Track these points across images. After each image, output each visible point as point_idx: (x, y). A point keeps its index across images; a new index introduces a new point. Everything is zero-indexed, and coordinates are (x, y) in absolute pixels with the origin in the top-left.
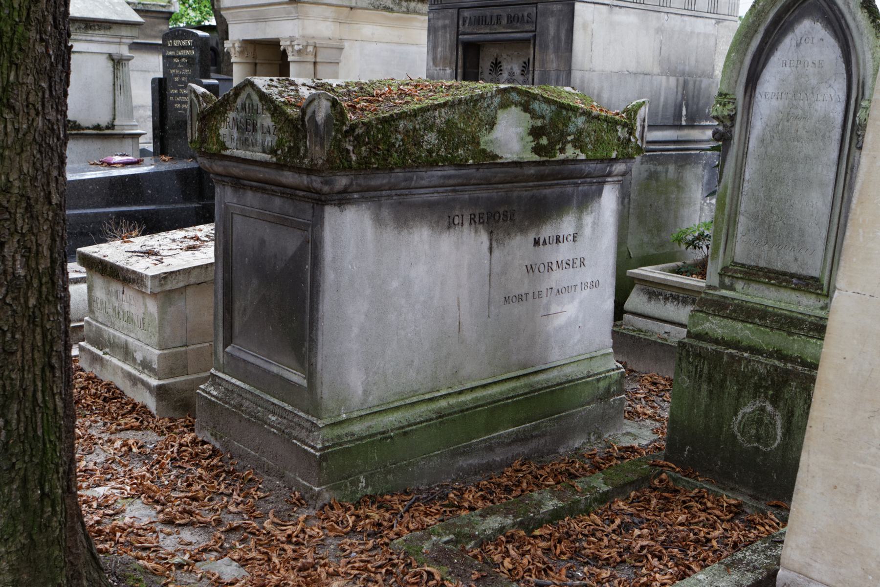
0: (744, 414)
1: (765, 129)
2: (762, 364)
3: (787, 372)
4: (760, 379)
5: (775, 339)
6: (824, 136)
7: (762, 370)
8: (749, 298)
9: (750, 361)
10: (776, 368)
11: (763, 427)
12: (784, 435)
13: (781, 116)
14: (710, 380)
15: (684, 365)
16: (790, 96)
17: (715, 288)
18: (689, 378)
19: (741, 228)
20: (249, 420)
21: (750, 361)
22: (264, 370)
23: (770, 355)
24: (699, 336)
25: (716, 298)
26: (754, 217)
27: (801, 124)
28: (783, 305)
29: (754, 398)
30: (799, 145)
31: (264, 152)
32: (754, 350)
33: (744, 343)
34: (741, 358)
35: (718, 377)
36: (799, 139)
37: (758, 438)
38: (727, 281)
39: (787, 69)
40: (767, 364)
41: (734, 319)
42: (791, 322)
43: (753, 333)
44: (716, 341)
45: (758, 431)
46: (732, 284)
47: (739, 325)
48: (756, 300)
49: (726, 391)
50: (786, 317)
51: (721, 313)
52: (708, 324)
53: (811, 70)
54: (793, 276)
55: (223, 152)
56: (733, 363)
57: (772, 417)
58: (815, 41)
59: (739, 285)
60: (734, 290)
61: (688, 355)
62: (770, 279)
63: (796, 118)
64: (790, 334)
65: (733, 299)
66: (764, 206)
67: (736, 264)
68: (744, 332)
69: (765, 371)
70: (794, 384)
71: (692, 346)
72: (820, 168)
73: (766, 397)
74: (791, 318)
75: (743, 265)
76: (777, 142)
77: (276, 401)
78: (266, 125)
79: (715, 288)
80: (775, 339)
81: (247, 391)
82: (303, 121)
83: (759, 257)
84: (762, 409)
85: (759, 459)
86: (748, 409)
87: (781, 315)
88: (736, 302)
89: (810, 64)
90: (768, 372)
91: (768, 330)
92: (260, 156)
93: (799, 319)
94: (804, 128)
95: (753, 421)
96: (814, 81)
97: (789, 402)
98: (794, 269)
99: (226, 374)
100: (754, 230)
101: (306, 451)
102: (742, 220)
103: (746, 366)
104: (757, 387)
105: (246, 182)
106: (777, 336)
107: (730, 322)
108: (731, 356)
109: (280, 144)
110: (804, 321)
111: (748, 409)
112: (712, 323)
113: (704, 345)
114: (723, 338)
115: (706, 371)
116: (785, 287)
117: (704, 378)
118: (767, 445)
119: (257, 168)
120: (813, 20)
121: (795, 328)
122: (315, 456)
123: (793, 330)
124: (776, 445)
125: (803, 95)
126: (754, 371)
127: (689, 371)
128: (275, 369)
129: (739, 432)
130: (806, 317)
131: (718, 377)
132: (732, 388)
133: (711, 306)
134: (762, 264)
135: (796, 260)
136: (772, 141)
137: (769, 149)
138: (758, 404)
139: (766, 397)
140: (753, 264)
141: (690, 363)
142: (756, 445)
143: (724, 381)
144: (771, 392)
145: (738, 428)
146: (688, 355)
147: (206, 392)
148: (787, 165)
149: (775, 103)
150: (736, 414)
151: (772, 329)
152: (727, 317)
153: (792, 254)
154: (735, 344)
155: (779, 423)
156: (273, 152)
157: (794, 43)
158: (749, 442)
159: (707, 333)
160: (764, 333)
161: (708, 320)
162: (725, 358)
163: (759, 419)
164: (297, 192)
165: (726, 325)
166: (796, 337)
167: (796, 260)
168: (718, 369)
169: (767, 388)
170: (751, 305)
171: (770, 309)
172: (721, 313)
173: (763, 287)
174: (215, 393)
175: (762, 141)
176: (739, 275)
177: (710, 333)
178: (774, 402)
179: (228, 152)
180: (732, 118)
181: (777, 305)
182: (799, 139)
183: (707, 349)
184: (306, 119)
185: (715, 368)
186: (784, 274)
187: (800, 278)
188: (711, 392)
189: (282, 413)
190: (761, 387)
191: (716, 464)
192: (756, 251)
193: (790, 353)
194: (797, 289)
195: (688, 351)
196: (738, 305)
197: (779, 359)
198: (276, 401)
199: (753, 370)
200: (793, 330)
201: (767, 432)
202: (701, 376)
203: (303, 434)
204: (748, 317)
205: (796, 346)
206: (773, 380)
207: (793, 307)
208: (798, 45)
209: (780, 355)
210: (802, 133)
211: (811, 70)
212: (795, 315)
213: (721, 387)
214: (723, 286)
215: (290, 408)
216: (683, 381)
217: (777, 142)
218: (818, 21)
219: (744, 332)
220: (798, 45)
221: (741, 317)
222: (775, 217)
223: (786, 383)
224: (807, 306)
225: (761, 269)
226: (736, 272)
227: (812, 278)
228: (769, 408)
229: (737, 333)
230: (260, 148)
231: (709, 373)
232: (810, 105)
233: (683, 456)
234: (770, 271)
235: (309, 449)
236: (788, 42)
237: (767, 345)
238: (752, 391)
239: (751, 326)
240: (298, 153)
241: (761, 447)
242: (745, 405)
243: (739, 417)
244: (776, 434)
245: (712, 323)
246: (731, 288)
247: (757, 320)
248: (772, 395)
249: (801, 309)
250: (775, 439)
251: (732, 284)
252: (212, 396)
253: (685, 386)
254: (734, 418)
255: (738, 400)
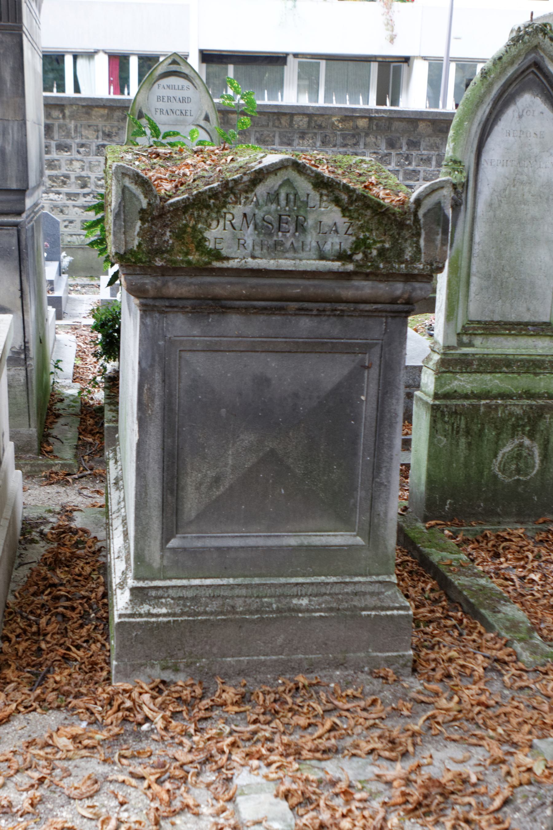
0: (504, 454)
1: (492, 194)
2: (517, 407)
3: (542, 407)
4: (518, 419)
5: (524, 382)
6: (548, 199)
7: (519, 411)
8: (491, 351)
9: (506, 406)
10: (531, 406)
11: (522, 461)
12: (542, 461)
13: (507, 181)
14: (468, 432)
15: (439, 426)
16: (515, 163)
17: (453, 348)
18: (445, 436)
19: (473, 288)
20: (261, 619)
21: (506, 406)
22: (269, 549)
23: (520, 397)
24: (447, 396)
25: (457, 357)
26: (487, 276)
27: (527, 189)
28: (524, 351)
29: (513, 437)
30: (526, 207)
31: (322, 257)
32: (503, 396)
33: (494, 392)
34: (497, 406)
35: (476, 428)
36: (525, 202)
37: (518, 471)
38: (465, 339)
39: (511, 138)
40: (522, 405)
41: (481, 373)
42: (534, 364)
43: (501, 380)
44: (466, 397)
45: (517, 465)
46: (470, 341)
47: (488, 377)
48: (499, 351)
49: (485, 438)
50: (528, 361)
51: (468, 370)
52: (456, 383)
53: (533, 140)
54: (527, 324)
55: (217, 264)
56: (490, 412)
57: (529, 449)
58: (536, 113)
59: (478, 341)
60: (473, 346)
61: (443, 415)
62: (509, 330)
63: (522, 183)
64: (536, 374)
65: (473, 355)
66: (496, 265)
67: (472, 322)
68: (494, 382)
69: (522, 411)
70: (548, 416)
71: (447, 406)
72: (546, 227)
73: (524, 434)
74: (532, 361)
75: (479, 322)
76: (505, 206)
77: (301, 580)
78: (327, 220)
79: (453, 348)
80: (524, 382)
81: (231, 587)
82: (416, 214)
83: (493, 312)
84: (521, 445)
85: (520, 490)
86: (507, 449)
87: (521, 361)
88: (477, 356)
89: (533, 135)
90: (524, 411)
91: (516, 375)
92: (312, 264)
93: (539, 361)
94: (530, 192)
95: (512, 457)
96: (536, 150)
97: (545, 432)
98: (527, 318)
99: (170, 579)
100: (487, 288)
101: (392, 616)
102: (474, 279)
103: (503, 411)
104: (514, 427)
105: (229, 303)
106: (524, 379)
107: (478, 376)
108: (488, 406)
109: (359, 245)
110: (543, 361)
111: (507, 449)
112: (461, 381)
113: (454, 402)
114: (472, 392)
115: (463, 426)
116: (525, 335)
117: (461, 432)
118: (527, 475)
119: (291, 282)
120: (533, 94)
121: (540, 368)
122: (407, 616)
123: (538, 371)
124: (535, 472)
125: (527, 163)
126: (511, 414)
127: (445, 430)
128: (293, 541)
129: (500, 471)
130: (543, 358)
131: (476, 428)
132: (490, 433)
133: (456, 365)
134: (497, 318)
135: (528, 310)
136: (500, 206)
137: (498, 212)
138: (517, 442)
139: (524, 434)
140: (488, 319)
141: (445, 422)
142: (516, 477)
143: (481, 430)
144: (528, 428)
145: (499, 468)
146: (443, 415)
147: (140, 615)
148: (515, 227)
149: (501, 170)
150: (495, 456)
151: (519, 373)
152: (475, 372)
153: (525, 305)
154: (486, 395)
155: (537, 452)
156: (342, 257)
157: (516, 114)
158: (510, 477)
159: (456, 391)
160: (512, 378)
161: (456, 379)
162: (482, 409)
163: (518, 455)
164: (362, 306)
165: (475, 380)
166: (542, 376)
167: (528, 310)
168: (475, 420)
169: (524, 426)
170: (491, 356)
171: (511, 357)
172: (468, 370)
173: (501, 339)
174: (164, 610)
175: (491, 205)
176: (480, 332)
177: (459, 391)
178: (531, 436)
179: (233, 264)
180: (465, 186)
181: (518, 352)
182: (525, 202)
183: (463, 405)
184: (421, 213)
185: (472, 420)
186: (519, 324)
187: (534, 324)
188: (469, 444)
189: (317, 591)
190: (518, 426)
191: (479, 506)
192: (490, 307)
193: (537, 391)
194: (536, 335)
195: (442, 412)
196: (480, 359)
197: (528, 398)
198: (301, 580)
199: (510, 414)
200: (538, 371)
201: (526, 463)
202: (458, 432)
203: (372, 601)
204: (495, 368)
205: (542, 384)
206: (529, 418)
207: (533, 352)
208: (520, 117)
209: (529, 395)
210: (528, 196)
211: (533, 140)
212: (533, 357)
213: (480, 436)
214: (461, 344)
215: (333, 579)
216: (440, 441)
217: (505, 206)
218: (537, 95)
219: (494, 382)
220: (520, 117)
221: (489, 369)
222: (507, 275)
223: (541, 416)
224: (543, 348)
225: (498, 323)
226: (474, 329)
227: (545, 323)
228: (527, 442)
229: (486, 384)
230: (313, 254)
231: (467, 427)
232: (534, 171)
233: (444, 511)
234: (506, 323)
235: (395, 612)
236: (510, 113)
237: (516, 389)
238: (510, 432)
239: (499, 375)
240: (401, 253)
241: (521, 478)
242: (504, 445)
243: (499, 458)
244: (535, 463)
245: (461, 381)
246: (470, 345)
247: (505, 369)
248: (529, 431)
249: (540, 352)
250: (533, 467)
251: (470, 341)
252: (164, 615)
253: (441, 446)
254: (494, 461)
255: (497, 443)
